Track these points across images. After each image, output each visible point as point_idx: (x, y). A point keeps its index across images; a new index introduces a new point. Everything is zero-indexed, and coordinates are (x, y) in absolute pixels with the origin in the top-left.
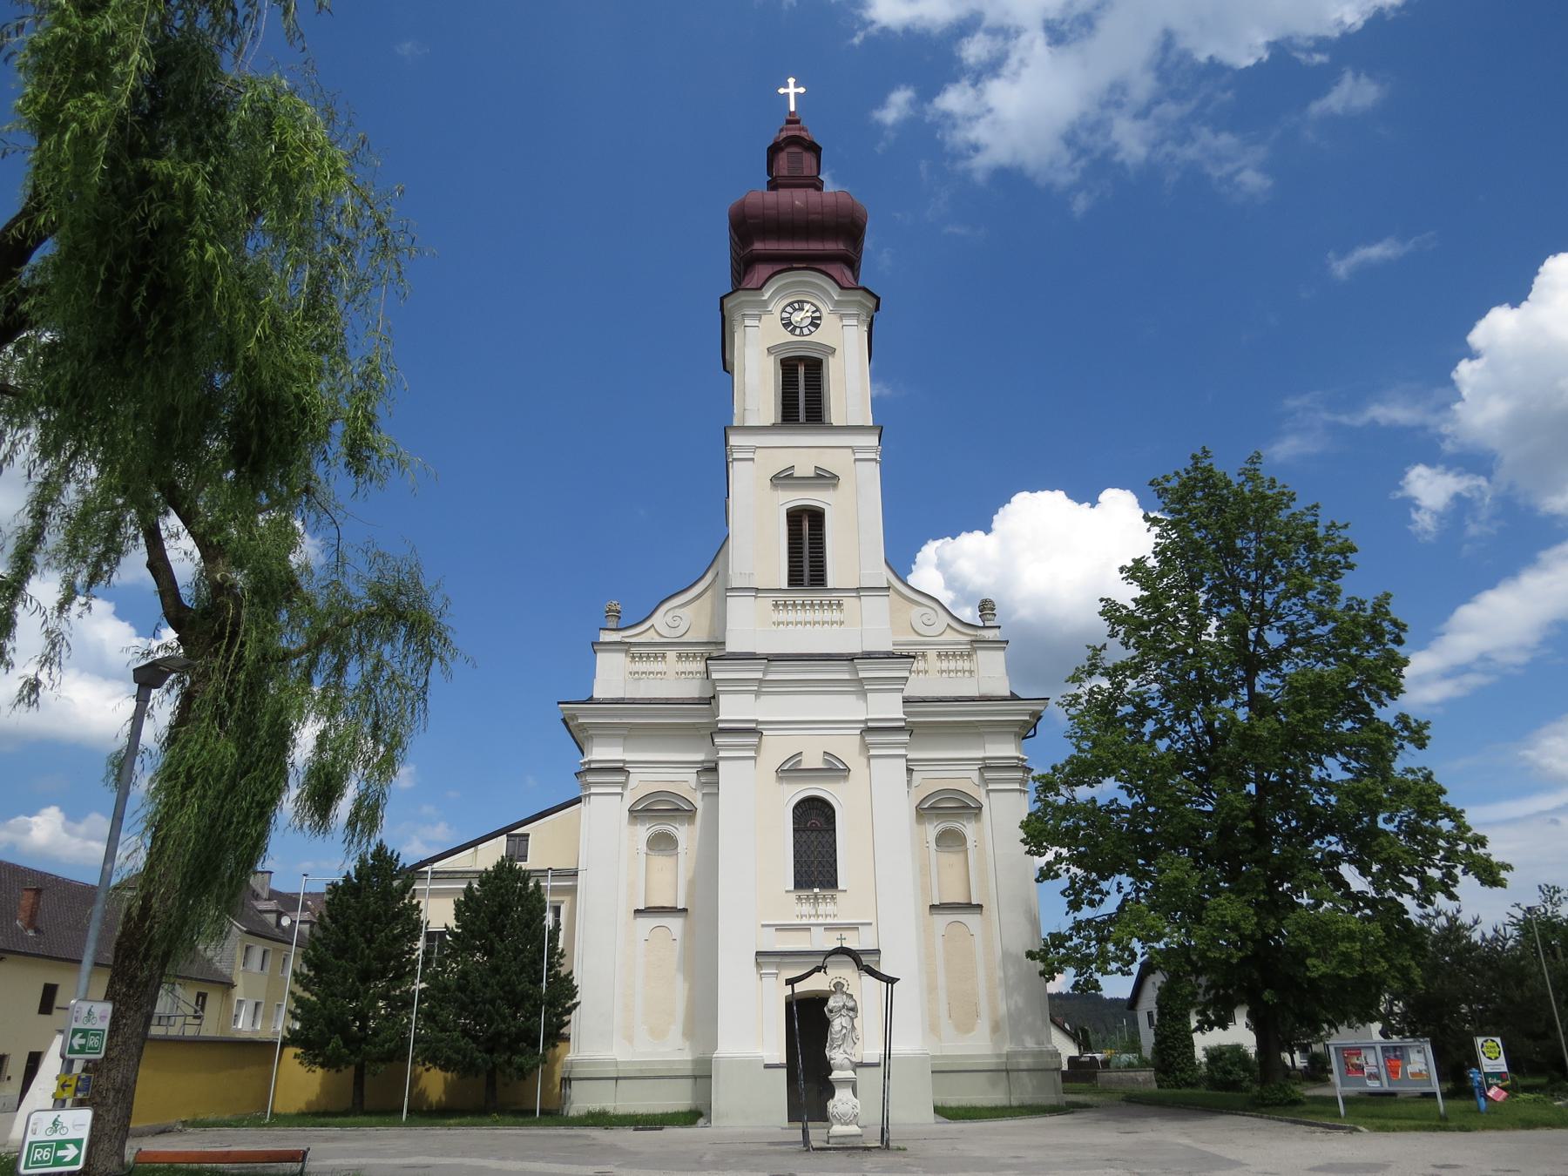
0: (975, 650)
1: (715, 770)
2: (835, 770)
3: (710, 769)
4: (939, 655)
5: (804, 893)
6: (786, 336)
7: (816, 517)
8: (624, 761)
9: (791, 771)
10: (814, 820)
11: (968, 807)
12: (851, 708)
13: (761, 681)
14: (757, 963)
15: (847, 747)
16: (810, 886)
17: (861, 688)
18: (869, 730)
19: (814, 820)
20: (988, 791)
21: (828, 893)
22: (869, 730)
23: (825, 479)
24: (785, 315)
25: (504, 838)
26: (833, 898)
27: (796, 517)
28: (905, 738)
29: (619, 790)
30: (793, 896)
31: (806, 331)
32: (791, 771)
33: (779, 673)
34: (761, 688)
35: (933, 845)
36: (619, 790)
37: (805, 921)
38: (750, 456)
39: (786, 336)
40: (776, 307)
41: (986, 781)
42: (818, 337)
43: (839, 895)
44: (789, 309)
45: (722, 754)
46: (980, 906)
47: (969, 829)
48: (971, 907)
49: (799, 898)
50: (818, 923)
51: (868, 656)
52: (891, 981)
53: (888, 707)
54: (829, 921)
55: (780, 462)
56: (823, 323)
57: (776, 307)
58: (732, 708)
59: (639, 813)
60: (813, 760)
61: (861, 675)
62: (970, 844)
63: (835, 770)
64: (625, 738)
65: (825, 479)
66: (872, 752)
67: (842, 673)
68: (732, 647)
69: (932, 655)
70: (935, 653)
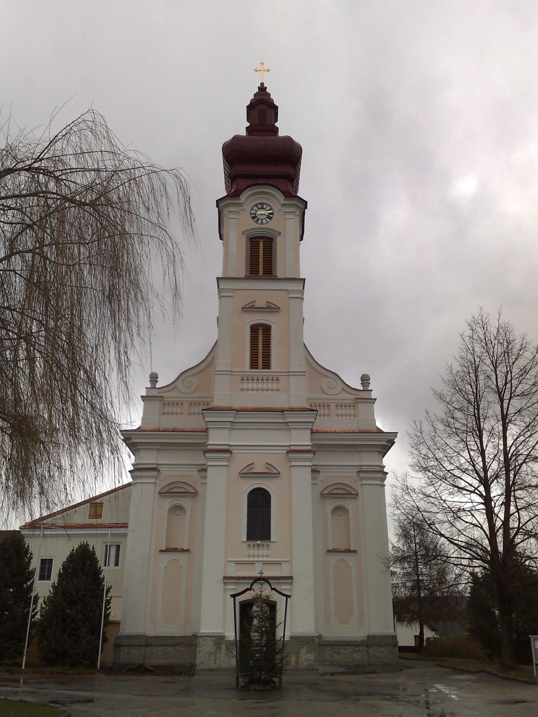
0: (357, 403)
1: (205, 470)
2: (272, 474)
3: (204, 470)
4: (337, 406)
5: (252, 543)
6: (253, 225)
7: (267, 329)
8: (157, 464)
9: (247, 474)
10: (259, 504)
11: (351, 494)
12: (282, 439)
13: (232, 422)
14: (225, 583)
15: (278, 461)
16: (256, 539)
17: (287, 426)
18: (290, 452)
19: (259, 504)
20: (362, 484)
21: (265, 543)
22: (290, 452)
23: (272, 308)
24: (253, 212)
25: (89, 504)
26: (268, 546)
27: (254, 329)
28: (311, 455)
29: (153, 481)
30: (246, 545)
31: (264, 221)
32: (247, 474)
33: (243, 418)
34: (233, 426)
35: (329, 515)
36: (153, 481)
37: (251, 559)
38: (231, 294)
39: (253, 225)
40: (247, 207)
41: (361, 479)
42: (271, 225)
43: (271, 545)
44: (255, 208)
45: (209, 463)
46: (355, 551)
47: (349, 505)
48: (348, 551)
49: (249, 546)
50: (259, 560)
51: (291, 410)
52: (288, 596)
53: (303, 439)
54: (265, 559)
55: (246, 300)
56: (275, 217)
57: (247, 207)
58: (217, 438)
59: (165, 493)
60: (260, 468)
61: (288, 420)
62: (350, 515)
63: (272, 474)
64: (158, 450)
65: (272, 308)
66: (293, 464)
67: (277, 418)
68: (216, 403)
69: (333, 406)
70: (335, 405)
